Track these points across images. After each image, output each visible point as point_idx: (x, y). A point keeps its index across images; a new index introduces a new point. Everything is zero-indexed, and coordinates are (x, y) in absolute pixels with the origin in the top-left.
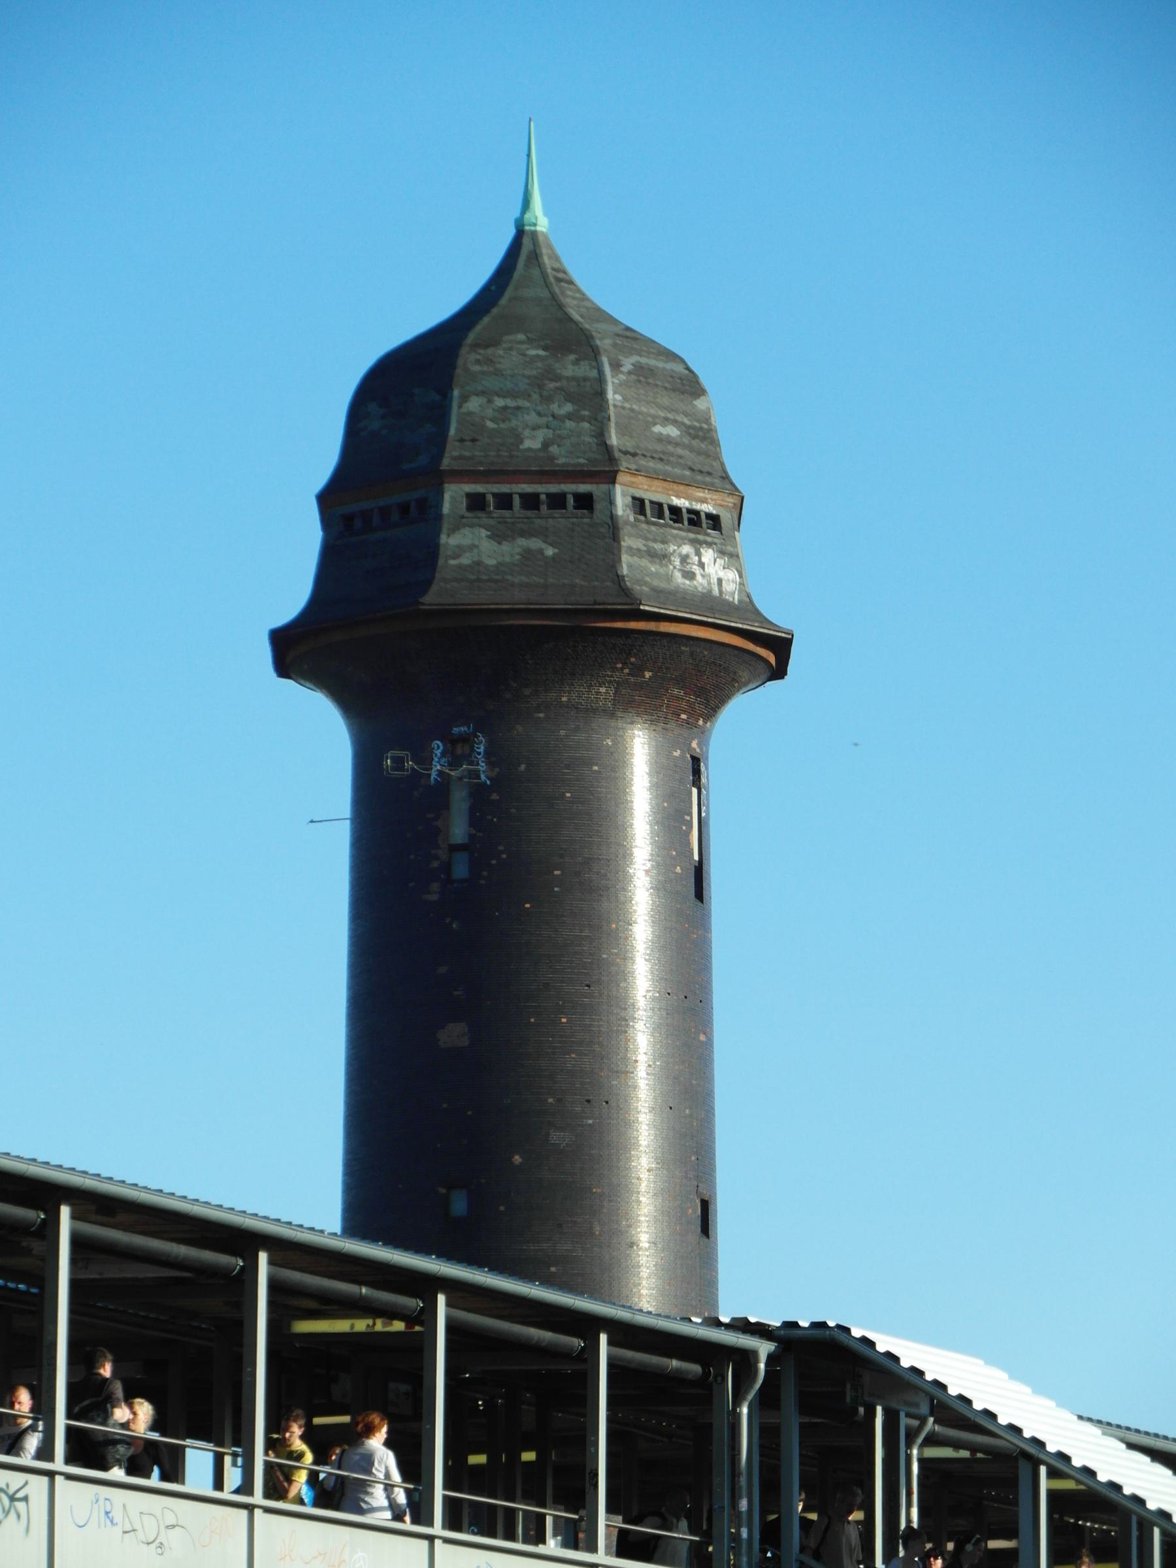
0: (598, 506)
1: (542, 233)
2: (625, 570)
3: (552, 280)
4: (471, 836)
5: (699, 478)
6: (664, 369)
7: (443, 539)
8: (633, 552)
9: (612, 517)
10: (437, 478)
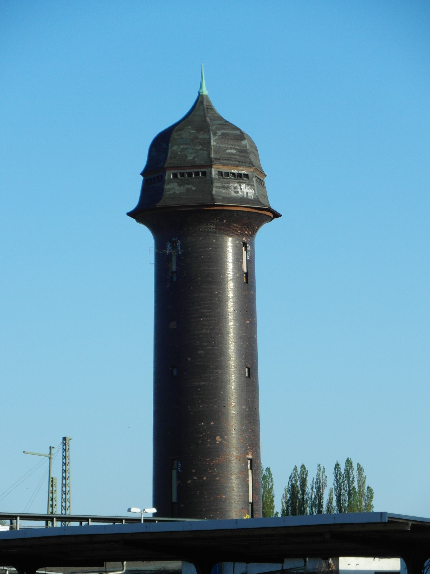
0: (207, 175)
1: (205, 95)
2: (214, 193)
3: (205, 109)
4: (177, 269)
5: (241, 164)
6: (233, 133)
7: (165, 186)
8: (217, 187)
9: (211, 178)
10: (164, 170)
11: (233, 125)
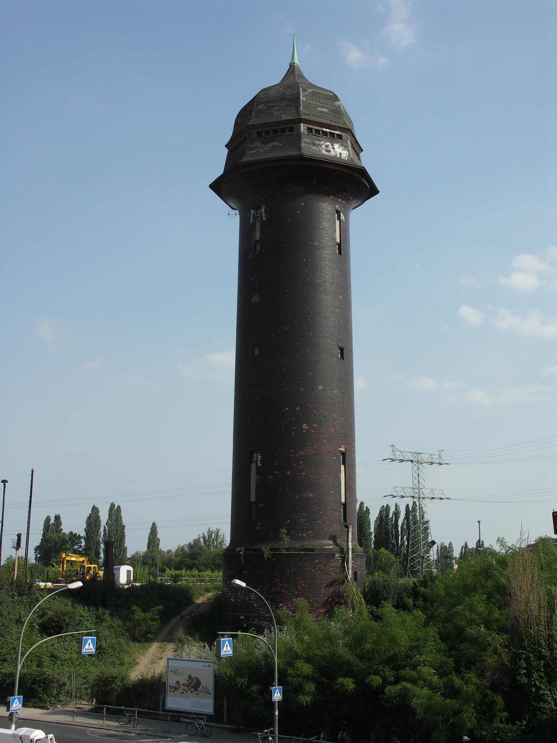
4: (260, 237)
8: (305, 142)
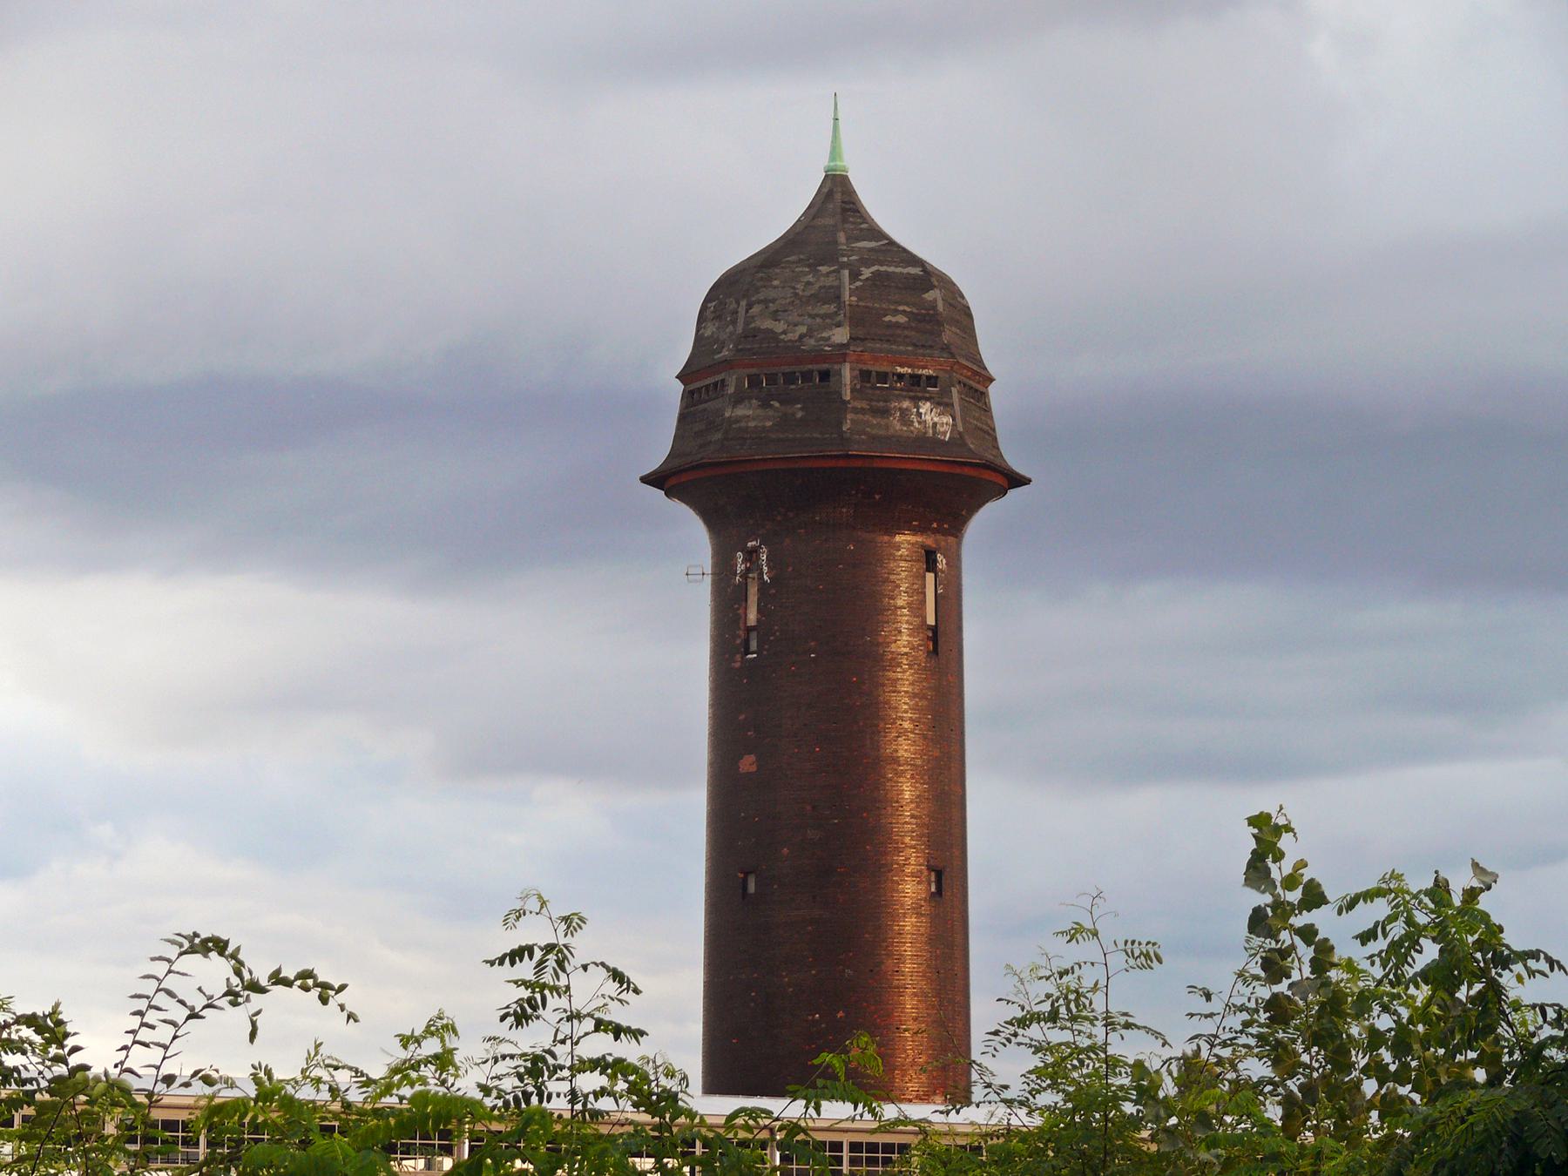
4: (758, 620)
11: (905, 250)
